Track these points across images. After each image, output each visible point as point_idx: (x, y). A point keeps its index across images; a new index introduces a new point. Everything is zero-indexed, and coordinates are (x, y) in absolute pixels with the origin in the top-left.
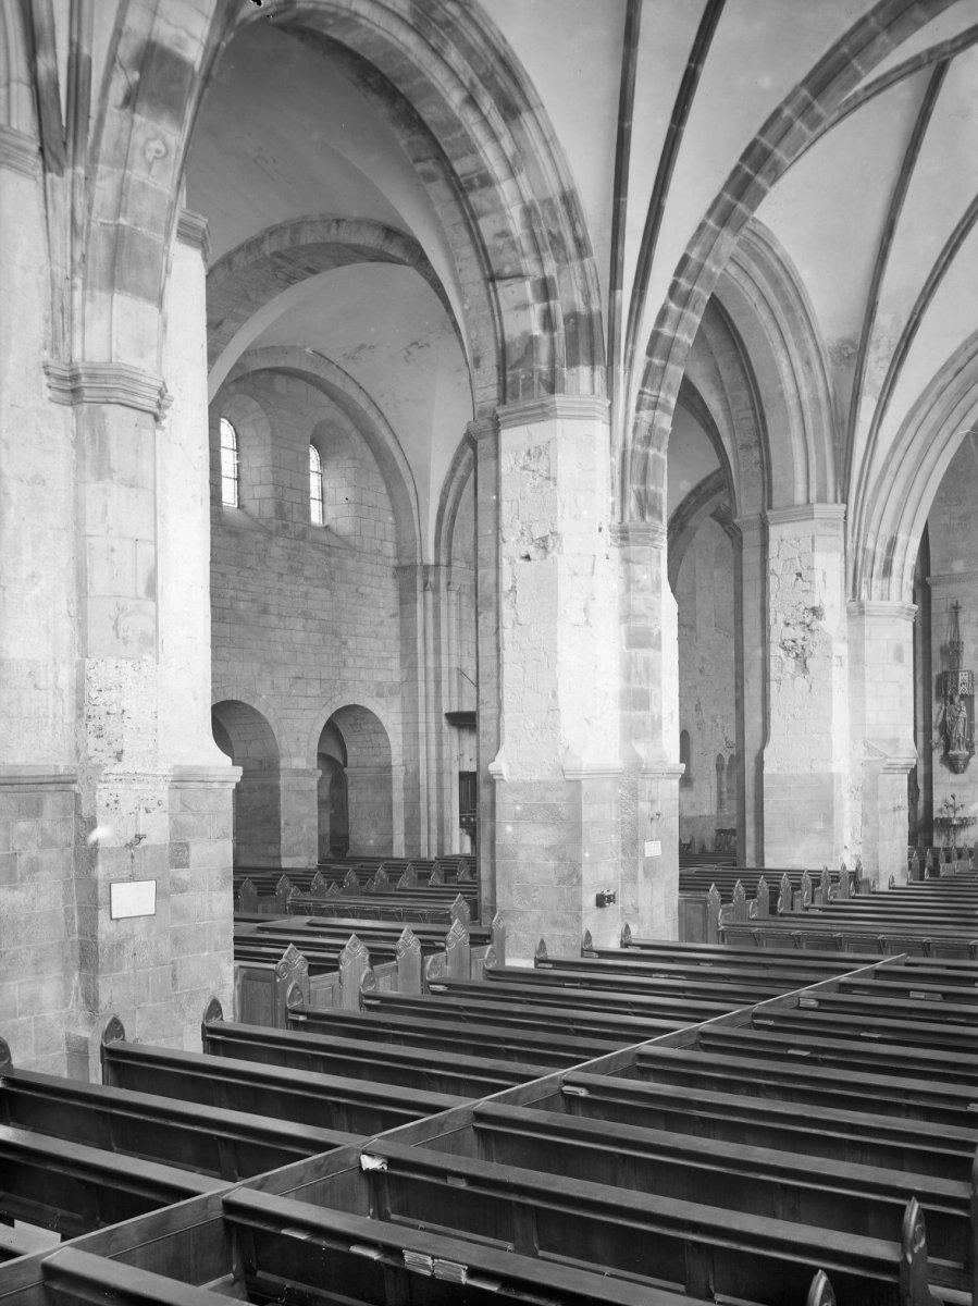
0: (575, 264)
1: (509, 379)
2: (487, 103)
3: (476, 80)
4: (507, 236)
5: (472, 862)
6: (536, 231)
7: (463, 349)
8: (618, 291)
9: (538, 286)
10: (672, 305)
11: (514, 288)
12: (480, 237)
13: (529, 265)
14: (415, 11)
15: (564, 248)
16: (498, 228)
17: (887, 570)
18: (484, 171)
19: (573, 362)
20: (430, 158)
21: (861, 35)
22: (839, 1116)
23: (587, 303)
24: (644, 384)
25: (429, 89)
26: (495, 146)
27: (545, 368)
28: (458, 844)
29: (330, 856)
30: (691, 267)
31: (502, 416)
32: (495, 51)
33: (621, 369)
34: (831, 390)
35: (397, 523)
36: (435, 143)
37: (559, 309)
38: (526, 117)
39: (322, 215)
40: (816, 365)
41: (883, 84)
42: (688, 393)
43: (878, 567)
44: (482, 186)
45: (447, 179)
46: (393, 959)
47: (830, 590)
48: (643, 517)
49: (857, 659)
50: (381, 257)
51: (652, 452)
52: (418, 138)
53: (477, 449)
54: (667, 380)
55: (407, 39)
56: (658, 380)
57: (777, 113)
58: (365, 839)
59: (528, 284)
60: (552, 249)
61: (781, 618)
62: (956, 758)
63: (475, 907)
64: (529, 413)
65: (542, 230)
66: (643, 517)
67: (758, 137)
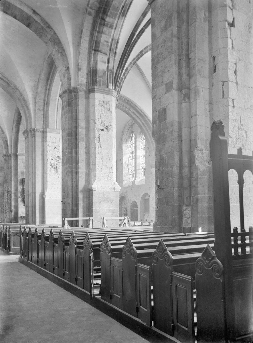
4: (108, 43)
11: (103, 56)
16: (106, 40)
18: (113, 24)
20: (94, 10)
22: (179, 248)
31: (96, 89)
44: (109, 27)
61: (51, 158)
64: (105, 91)
67: (143, 50)
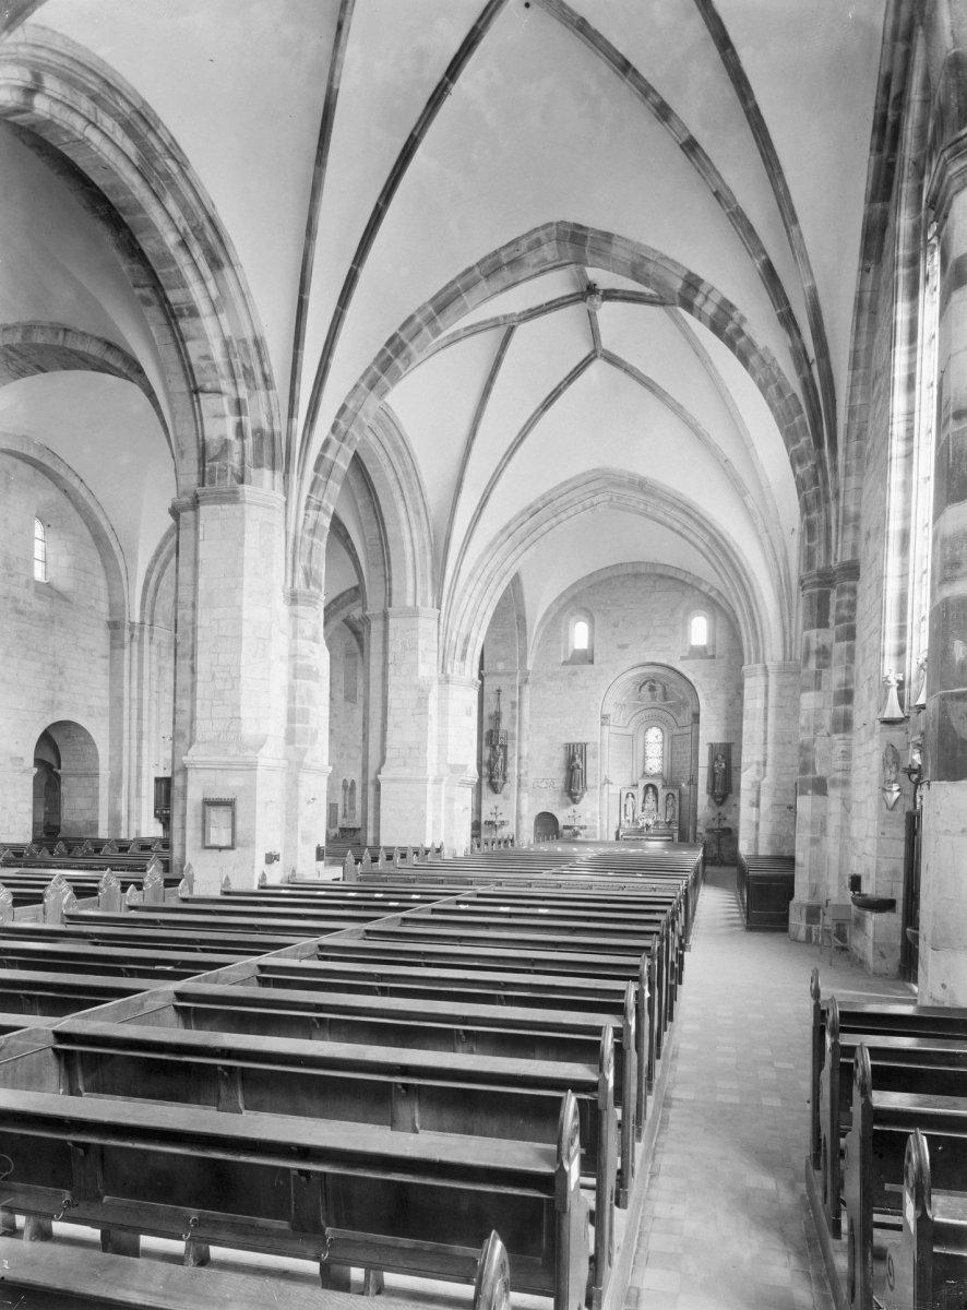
0: (262, 393)
1: (207, 469)
2: (197, 251)
3: (189, 230)
5: (166, 844)
6: (233, 361)
7: (169, 441)
8: (295, 419)
9: (233, 404)
10: (333, 438)
12: (188, 357)
13: (225, 385)
14: (140, 157)
15: (254, 379)
17: (464, 656)
19: (259, 466)
20: (146, 286)
21: (468, 278)
23: (271, 424)
24: (312, 490)
25: (150, 226)
26: (202, 286)
27: (237, 466)
28: (151, 829)
29: (44, 836)
30: (348, 414)
32: (206, 212)
33: (294, 477)
34: (360, 682)
35: (110, 588)
36: (152, 274)
37: (249, 428)
38: (227, 271)
39: (51, 323)
40: (423, 515)
41: (473, 330)
42: (337, 525)
43: (459, 653)
45: (162, 306)
46: (96, 895)
47: (427, 669)
48: (308, 585)
49: (443, 711)
50: (103, 367)
51: (316, 540)
52: (136, 267)
53: (176, 547)
54: (328, 491)
55: (132, 179)
56: (322, 490)
57: (411, 318)
58: (72, 812)
59: (225, 399)
60: (245, 378)
62: (496, 783)
63: (167, 866)
65: (237, 362)
66: (308, 585)
